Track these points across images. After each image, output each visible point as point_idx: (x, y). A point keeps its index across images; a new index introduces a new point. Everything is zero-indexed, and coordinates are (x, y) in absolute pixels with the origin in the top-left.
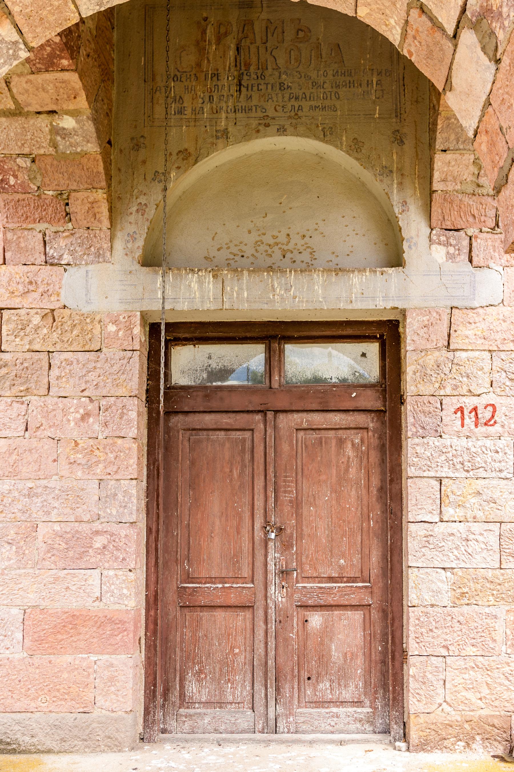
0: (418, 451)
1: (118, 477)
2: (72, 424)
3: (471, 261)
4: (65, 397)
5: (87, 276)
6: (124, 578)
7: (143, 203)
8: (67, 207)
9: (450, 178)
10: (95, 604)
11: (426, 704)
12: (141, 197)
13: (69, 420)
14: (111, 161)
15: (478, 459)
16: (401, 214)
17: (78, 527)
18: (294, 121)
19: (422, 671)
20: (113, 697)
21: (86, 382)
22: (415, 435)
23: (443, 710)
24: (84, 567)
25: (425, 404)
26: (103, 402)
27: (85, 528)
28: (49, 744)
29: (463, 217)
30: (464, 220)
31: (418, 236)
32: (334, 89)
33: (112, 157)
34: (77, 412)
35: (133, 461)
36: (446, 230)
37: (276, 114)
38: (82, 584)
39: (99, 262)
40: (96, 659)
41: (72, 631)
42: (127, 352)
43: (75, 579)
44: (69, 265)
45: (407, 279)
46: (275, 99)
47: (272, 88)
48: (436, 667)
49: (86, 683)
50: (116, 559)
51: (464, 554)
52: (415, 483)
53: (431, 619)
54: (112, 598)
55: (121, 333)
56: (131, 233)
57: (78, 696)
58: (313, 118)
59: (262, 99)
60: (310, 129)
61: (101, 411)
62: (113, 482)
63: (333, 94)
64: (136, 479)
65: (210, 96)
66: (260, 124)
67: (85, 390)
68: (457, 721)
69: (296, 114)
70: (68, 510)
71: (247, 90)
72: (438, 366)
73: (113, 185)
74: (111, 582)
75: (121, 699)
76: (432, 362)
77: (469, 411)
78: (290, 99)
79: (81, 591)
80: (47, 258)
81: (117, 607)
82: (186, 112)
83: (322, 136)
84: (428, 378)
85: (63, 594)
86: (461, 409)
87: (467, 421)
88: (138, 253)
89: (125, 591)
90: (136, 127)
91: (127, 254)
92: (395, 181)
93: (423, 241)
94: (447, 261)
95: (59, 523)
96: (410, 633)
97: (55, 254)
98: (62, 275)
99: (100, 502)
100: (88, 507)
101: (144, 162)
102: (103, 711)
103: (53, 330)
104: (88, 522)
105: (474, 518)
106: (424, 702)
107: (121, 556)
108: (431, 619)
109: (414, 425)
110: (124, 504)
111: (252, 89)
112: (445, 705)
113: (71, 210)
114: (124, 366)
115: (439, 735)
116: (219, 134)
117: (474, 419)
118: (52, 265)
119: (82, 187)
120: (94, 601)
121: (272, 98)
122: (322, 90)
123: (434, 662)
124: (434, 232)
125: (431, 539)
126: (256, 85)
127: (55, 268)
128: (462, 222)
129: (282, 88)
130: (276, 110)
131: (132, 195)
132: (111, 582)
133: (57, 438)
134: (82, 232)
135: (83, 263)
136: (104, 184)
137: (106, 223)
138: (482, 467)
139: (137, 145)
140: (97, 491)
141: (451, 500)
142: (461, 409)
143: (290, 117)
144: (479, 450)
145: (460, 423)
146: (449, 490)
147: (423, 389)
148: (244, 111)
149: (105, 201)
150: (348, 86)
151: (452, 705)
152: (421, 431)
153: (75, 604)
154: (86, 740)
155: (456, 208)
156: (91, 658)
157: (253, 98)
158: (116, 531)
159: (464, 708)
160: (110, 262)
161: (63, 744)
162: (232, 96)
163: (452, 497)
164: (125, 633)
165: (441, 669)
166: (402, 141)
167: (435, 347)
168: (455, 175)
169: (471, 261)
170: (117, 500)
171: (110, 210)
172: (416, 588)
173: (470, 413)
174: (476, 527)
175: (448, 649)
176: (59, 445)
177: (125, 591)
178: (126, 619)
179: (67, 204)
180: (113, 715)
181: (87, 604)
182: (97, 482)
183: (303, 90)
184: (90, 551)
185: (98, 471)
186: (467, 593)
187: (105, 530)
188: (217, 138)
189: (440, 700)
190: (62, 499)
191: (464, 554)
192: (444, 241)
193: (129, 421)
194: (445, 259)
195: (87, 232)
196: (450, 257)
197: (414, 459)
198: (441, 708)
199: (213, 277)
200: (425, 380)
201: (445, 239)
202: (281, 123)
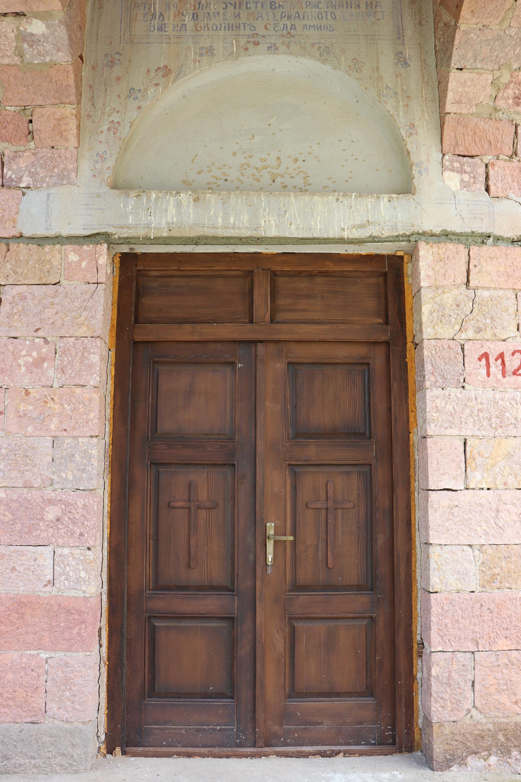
0: (438, 405)
1: (75, 433)
2: (23, 369)
3: (487, 190)
4: (16, 338)
5: (48, 199)
6: (82, 558)
7: (115, 121)
8: (30, 125)
9: (464, 100)
10: (45, 589)
11: (452, 710)
12: (114, 115)
13: (19, 366)
14: (82, 77)
15: (508, 414)
16: (409, 137)
17: (27, 494)
18: (286, 40)
19: (447, 670)
20: (68, 703)
21: (41, 320)
22: (434, 384)
23: (471, 717)
24: (33, 543)
25: (444, 349)
26: (61, 344)
27: (34, 495)
29: (478, 143)
30: (479, 146)
31: (428, 161)
32: (330, 10)
33: (83, 74)
34: (30, 355)
35: (94, 415)
36: (459, 155)
37: (266, 33)
38: (31, 564)
39: (62, 185)
40: (48, 656)
41: (18, 622)
42: (91, 285)
43: (23, 558)
44: (29, 188)
45: (418, 207)
46: (265, 18)
47: (262, 6)
48: (463, 665)
49: (35, 687)
50: (72, 534)
51: (493, 528)
52: (435, 443)
53: (457, 608)
54: (66, 582)
55: (84, 264)
56: (101, 153)
57: (26, 701)
58: (307, 37)
59: (251, 18)
60: (304, 48)
61: (57, 355)
62: (68, 441)
63: (329, 14)
64: (96, 436)
65: (193, 14)
66: (248, 42)
67: (39, 329)
68: (489, 730)
69: (289, 33)
70: (15, 473)
71: (235, 8)
72: (458, 306)
73: (82, 102)
74: (66, 562)
75: (78, 707)
76: (450, 301)
77: (495, 358)
78: (282, 18)
79: (30, 573)
80: (5, 181)
81: (73, 593)
82: (166, 29)
83: (318, 55)
84: (447, 319)
85: (8, 576)
86: (486, 356)
87: (492, 369)
88: (107, 175)
89: (83, 574)
90: (111, 43)
91: (94, 176)
92: (401, 103)
94: (461, 189)
95: (4, 489)
96: (432, 624)
97: (13, 176)
98: (20, 200)
99: (54, 464)
100: (39, 469)
101: (119, 79)
102: (57, 722)
103: (6, 260)
104: (39, 488)
105: (505, 484)
106: (450, 709)
107: (78, 531)
108: (457, 608)
109: (433, 374)
110: (82, 467)
111: (240, 7)
112: (474, 712)
113: (35, 127)
114: (86, 301)
115: (467, 748)
116: (204, 52)
117: (501, 368)
118: (9, 187)
119: (48, 101)
120: (46, 585)
121: (261, 17)
122: (317, 10)
123: (462, 660)
124: (447, 157)
125: (455, 510)
126: (245, 3)
127: (13, 192)
128: (476, 148)
129: (273, 7)
130: (266, 29)
131: (103, 113)
132: (66, 562)
133: (4, 387)
134: (46, 152)
135: (45, 185)
136: (73, 98)
137: (73, 142)
138: (512, 424)
139: (112, 62)
140: (50, 451)
141: (478, 464)
142: (486, 356)
143: (282, 36)
144: (508, 403)
145: (485, 371)
146: (475, 451)
147: (441, 331)
148: (231, 29)
149: (74, 117)
150: (345, 7)
151: (483, 711)
152: (440, 380)
153: (22, 589)
154: (33, 758)
155: (470, 133)
156: (42, 655)
157: (241, 16)
158: (73, 500)
159: (497, 714)
160: (75, 184)
161: (6, 762)
162: (218, 13)
163: (479, 460)
164: (83, 626)
165: (469, 668)
166: (406, 63)
167: (453, 283)
168: (471, 97)
169: (487, 190)
170: (74, 461)
171: (79, 127)
172: (438, 570)
173: (496, 360)
175: (478, 643)
176: (6, 395)
177: (83, 574)
178: (84, 609)
179: (31, 121)
180: (67, 726)
181: (37, 589)
182: (50, 439)
183: (296, 10)
184: (41, 524)
185: (52, 427)
186: (499, 574)
187: (59, 498)
188: (201, 55)
189: (468, 705)
190: (8, 460)
191: (493, 528)
192: (458, 168)
193: (91, 366)
194: (459, 187)
195: (51, 152)
196: (465, 185)
197: (434, 414)
198: (470, 715)
199: (194, 200)
200: (444, 321)
201: (458, 165)
202: (272, 41)
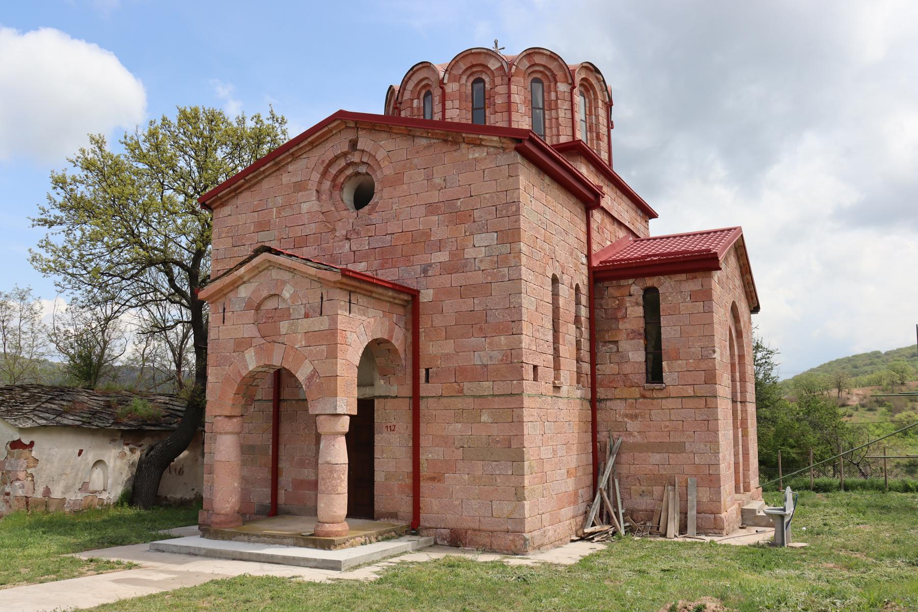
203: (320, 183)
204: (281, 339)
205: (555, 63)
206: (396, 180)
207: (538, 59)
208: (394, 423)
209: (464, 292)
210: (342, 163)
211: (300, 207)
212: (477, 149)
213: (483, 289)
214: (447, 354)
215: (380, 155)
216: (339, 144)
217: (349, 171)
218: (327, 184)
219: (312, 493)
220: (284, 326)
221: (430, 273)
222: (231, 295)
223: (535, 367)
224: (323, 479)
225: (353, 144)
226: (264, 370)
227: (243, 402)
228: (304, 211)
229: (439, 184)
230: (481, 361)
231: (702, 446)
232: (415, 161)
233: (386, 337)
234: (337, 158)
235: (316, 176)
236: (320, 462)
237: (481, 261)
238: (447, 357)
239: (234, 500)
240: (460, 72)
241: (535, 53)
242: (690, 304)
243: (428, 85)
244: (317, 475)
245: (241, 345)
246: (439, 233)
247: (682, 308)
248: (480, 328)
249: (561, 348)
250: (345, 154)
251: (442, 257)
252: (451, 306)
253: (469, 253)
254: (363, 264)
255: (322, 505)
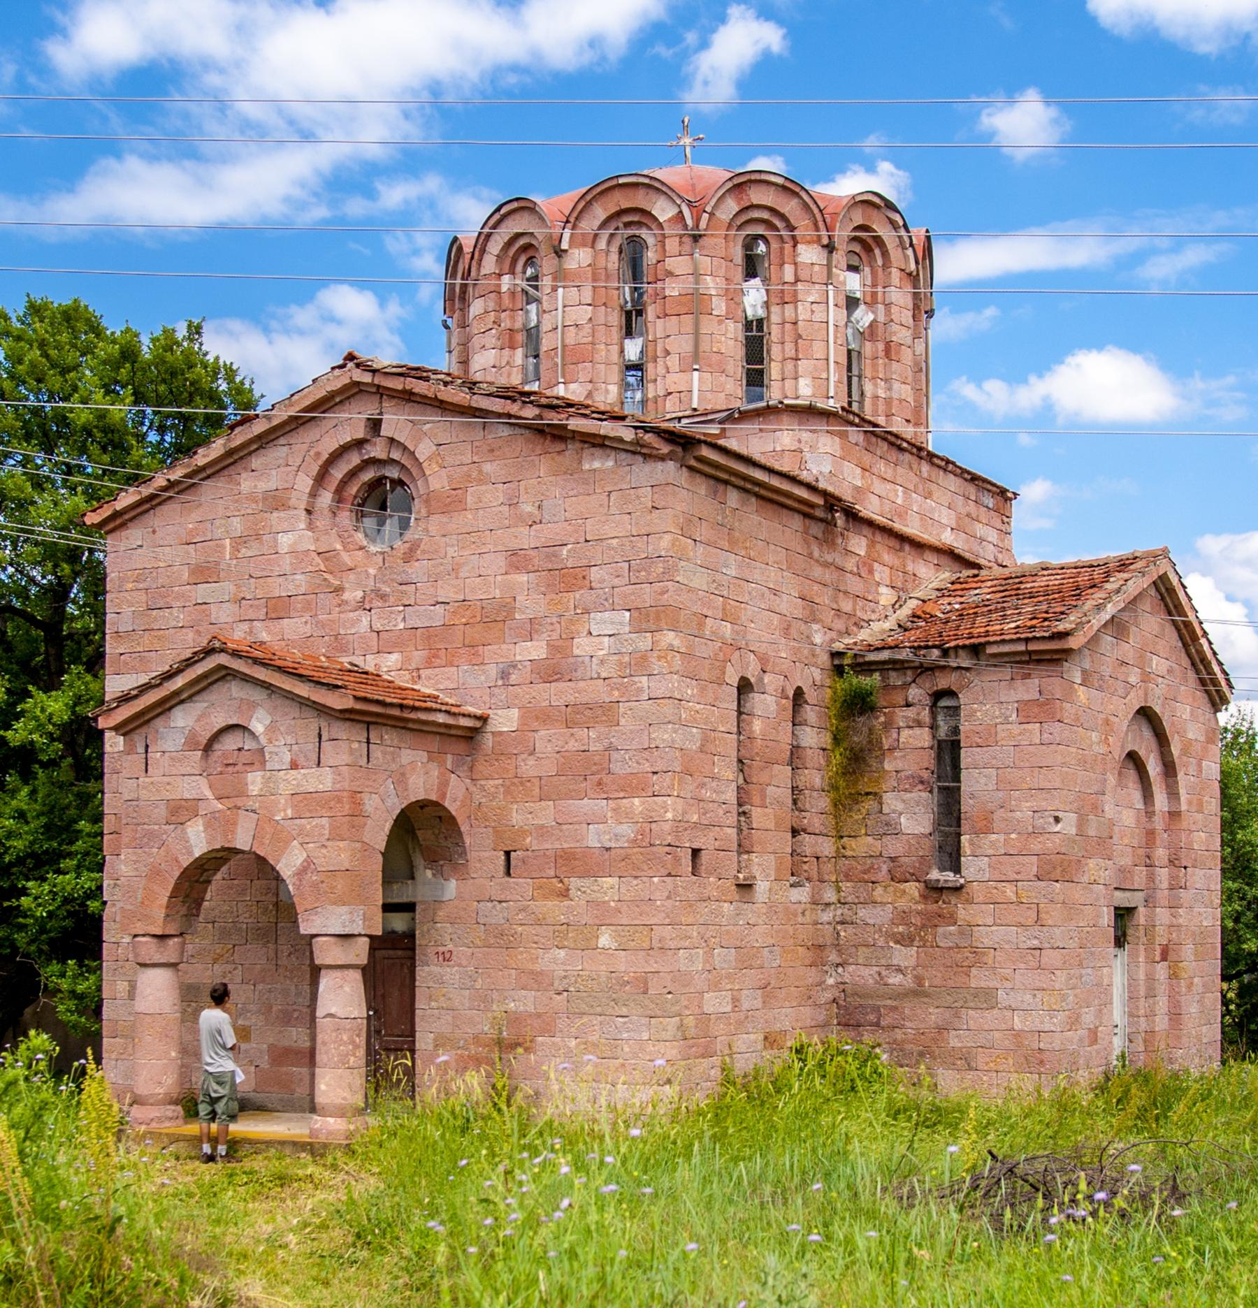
27: (290, 1008)
28: (279, 1108)
93: (421, 867)
174: (443, 1012)
203: (313, 494)
204: (250, 804)
205: (794, 202)
206: (452, 503)
207: (758, 196)
208: (450, 947)
209: (576, 716)
210: (354, 459)
211: (276, 540)
212: (598, 452)
213: (605, 713)
214: (542, 826)
215: (424, 450)
216: (347, 424)
217: (368, 475)
218: (326, 498)
219: (305, 1070)
220: (255, 781)
221: (513, 678)
222: (158, 723)
223: (696, 853)
224: (324, 1043)
225: (375, 425)
226: (220, 854)
227: (184, 911)
228: (283, 549)
229: (530, 514)
230: (599, 841)
231: (1028, 997)
232: (487, 467)
233: (434, 798)
234: (344, 449)
235: (305, 483)
236: (318, 1014)
237: (602, 662)
238: (542, 831)
239: (170, 1081)
240: (597, 223)
241: (750, 181)
242: (1016, 729)
243: (528, 247)
244: (313, 1038)
245: (180, 812)
246: (530, 604)
247: (1001, 735)
248: (599, 784)
249: (756, 812)
250: (359, 444)
251: (536, 650)
252: (547, 740)
253: (582, 646)
254: (395, 657)
255: (323, 1087)
